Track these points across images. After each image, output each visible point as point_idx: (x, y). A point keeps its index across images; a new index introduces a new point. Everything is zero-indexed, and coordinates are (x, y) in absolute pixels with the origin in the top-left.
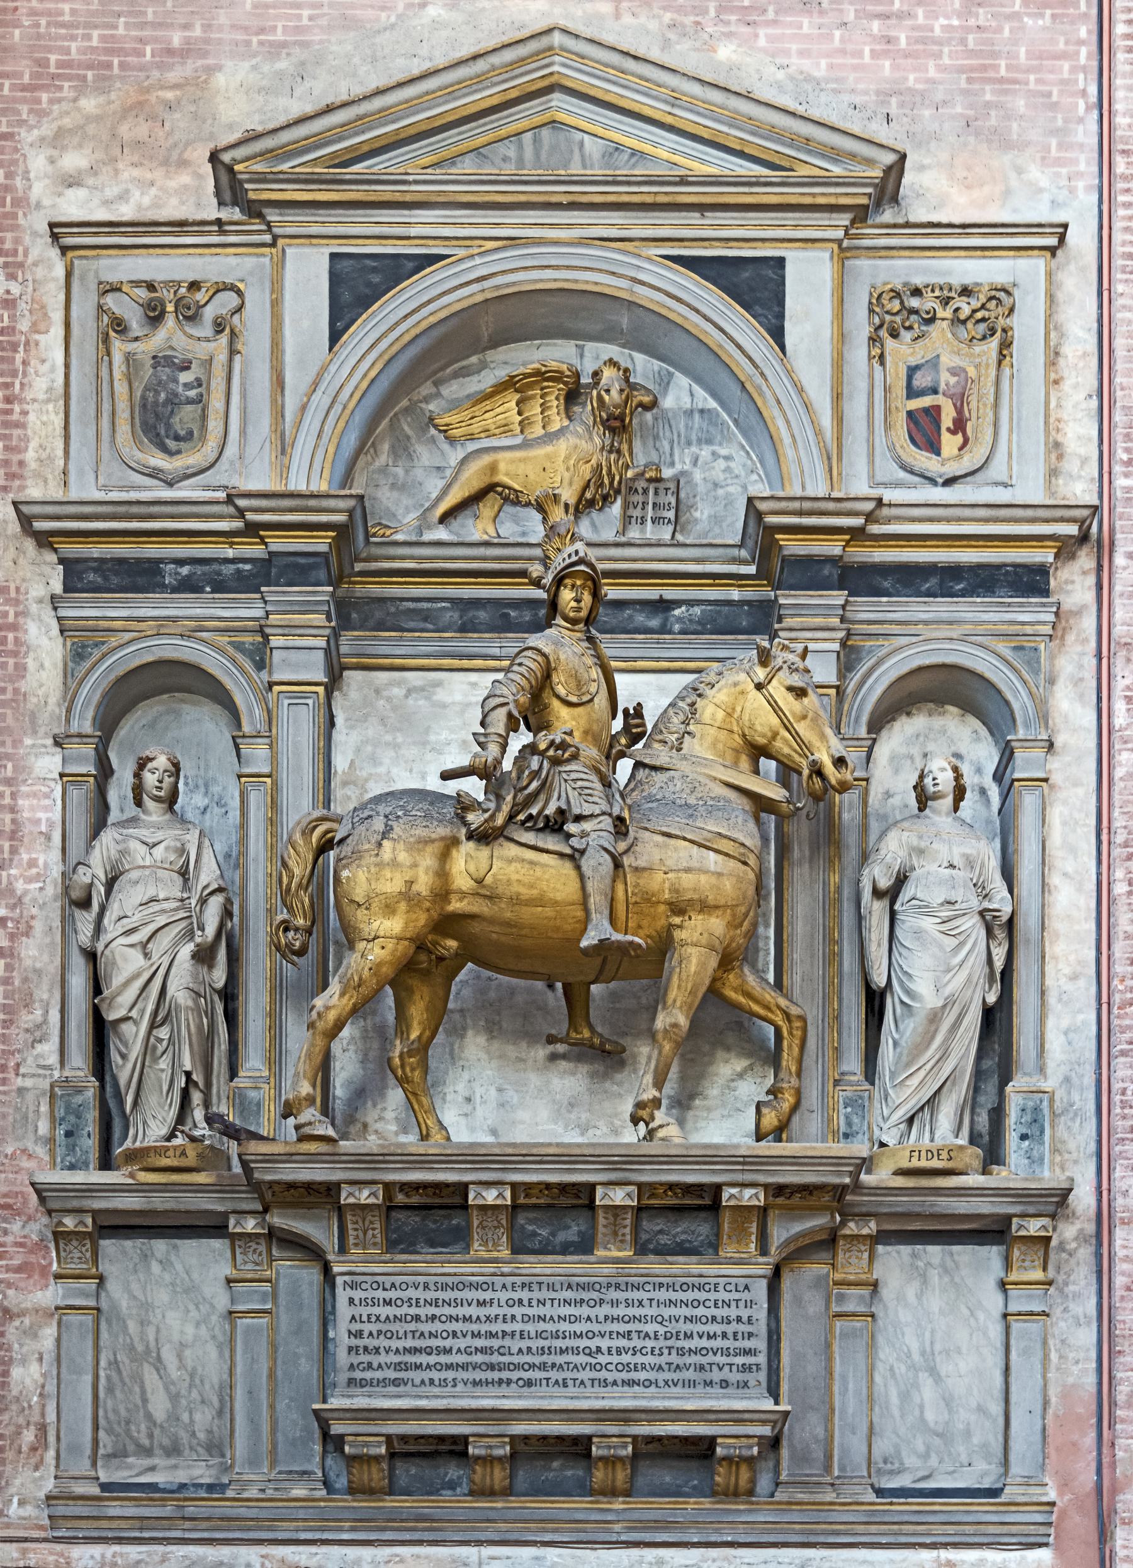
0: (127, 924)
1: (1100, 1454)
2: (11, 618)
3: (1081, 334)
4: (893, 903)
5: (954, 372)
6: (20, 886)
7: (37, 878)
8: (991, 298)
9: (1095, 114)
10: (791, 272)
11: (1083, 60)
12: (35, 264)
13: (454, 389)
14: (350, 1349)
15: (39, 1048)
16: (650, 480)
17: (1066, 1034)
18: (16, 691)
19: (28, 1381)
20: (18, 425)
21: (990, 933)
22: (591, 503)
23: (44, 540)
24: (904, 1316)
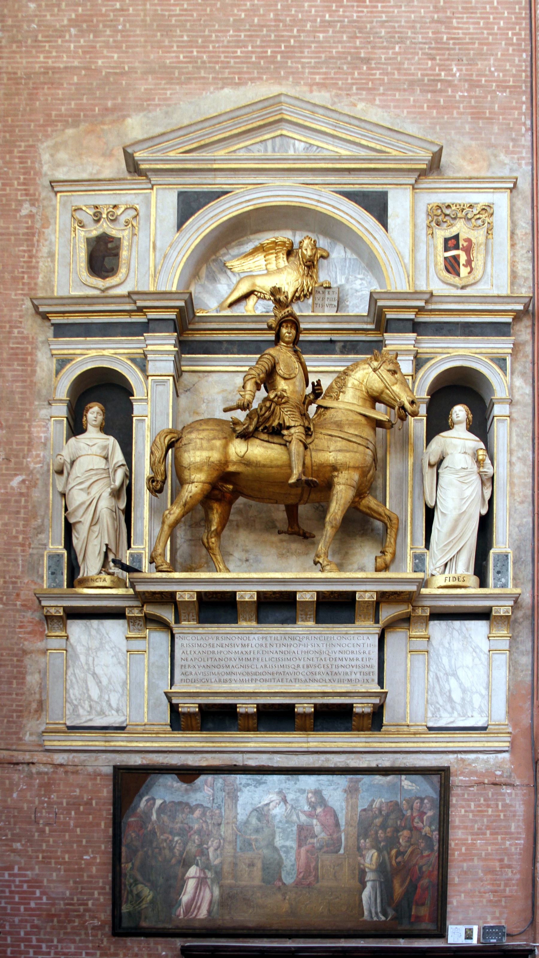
0: (79, 480)
1: (532, 711)
2: (30, 350)
3: (524, 225)
4: (438, 469)
5: (465, 240)
6: (32, 466)
7: (39, 462)
8: (483, 209)
9: (530, 133)
10: (390, 195)
11: (524, 110)
12: (44, 199)
13: (234, 251)
14: (182, 666)
15: (40, 536)
16: (326, 288)
17: (518, 527)
18: (32, 381)
19: (34, 681)
20: (34, 267)
21: (483, 483)
22: (298, 298)
23: (45, 316)
24: (442, 651)
